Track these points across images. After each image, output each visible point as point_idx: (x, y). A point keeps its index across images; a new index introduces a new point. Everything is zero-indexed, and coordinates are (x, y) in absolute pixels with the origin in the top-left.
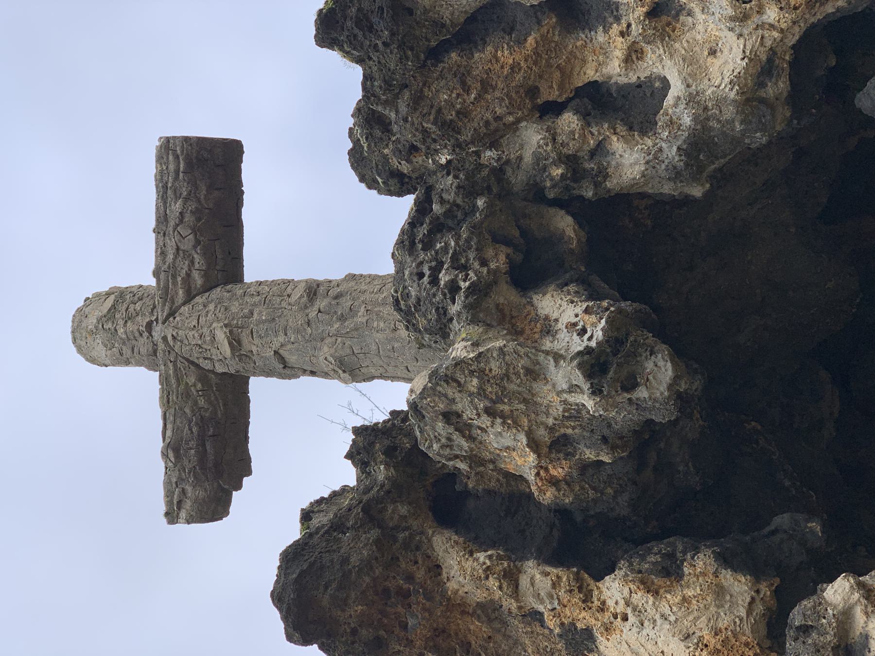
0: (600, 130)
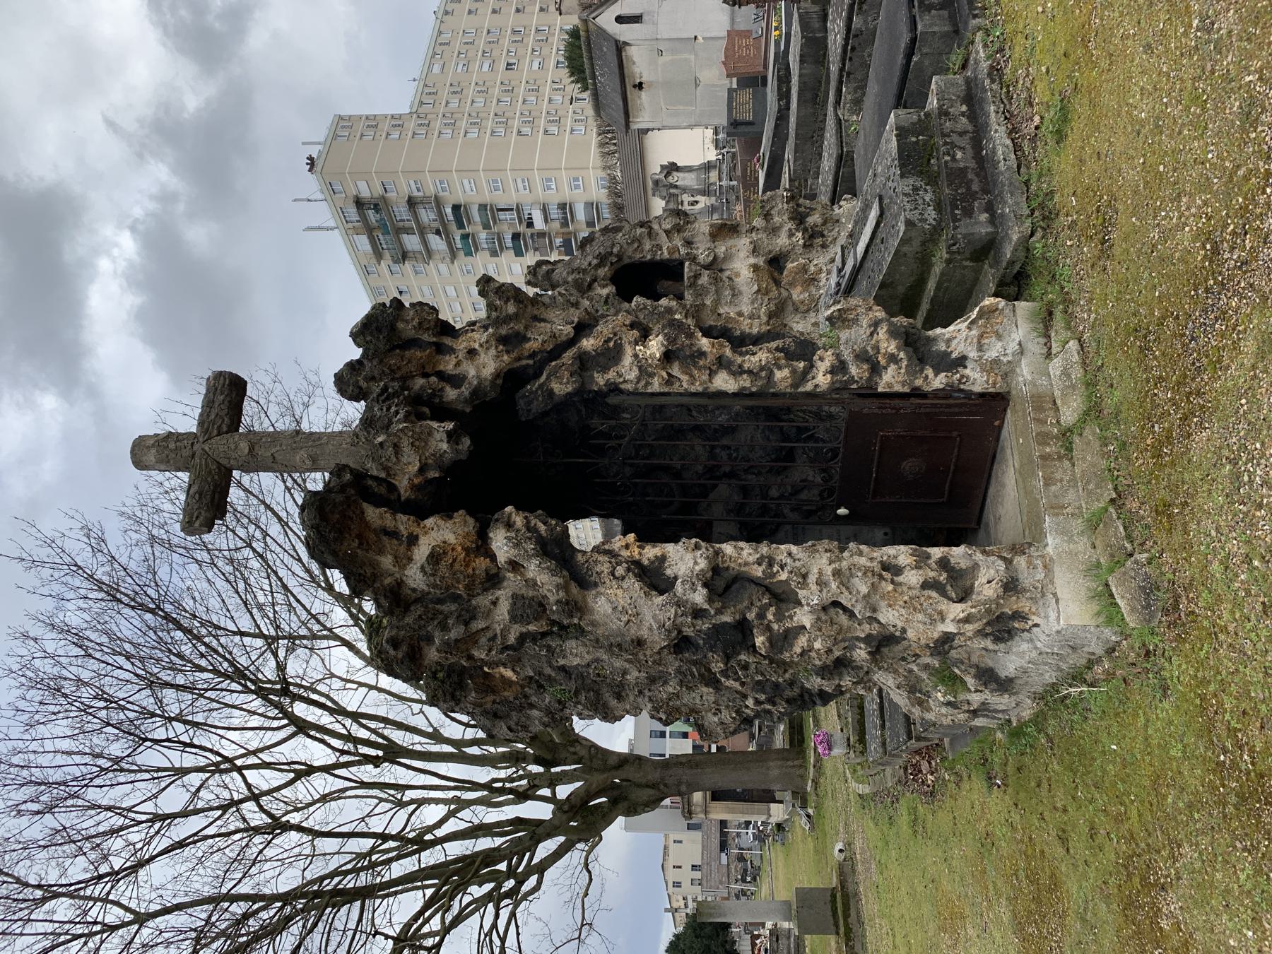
0: (442, 384)
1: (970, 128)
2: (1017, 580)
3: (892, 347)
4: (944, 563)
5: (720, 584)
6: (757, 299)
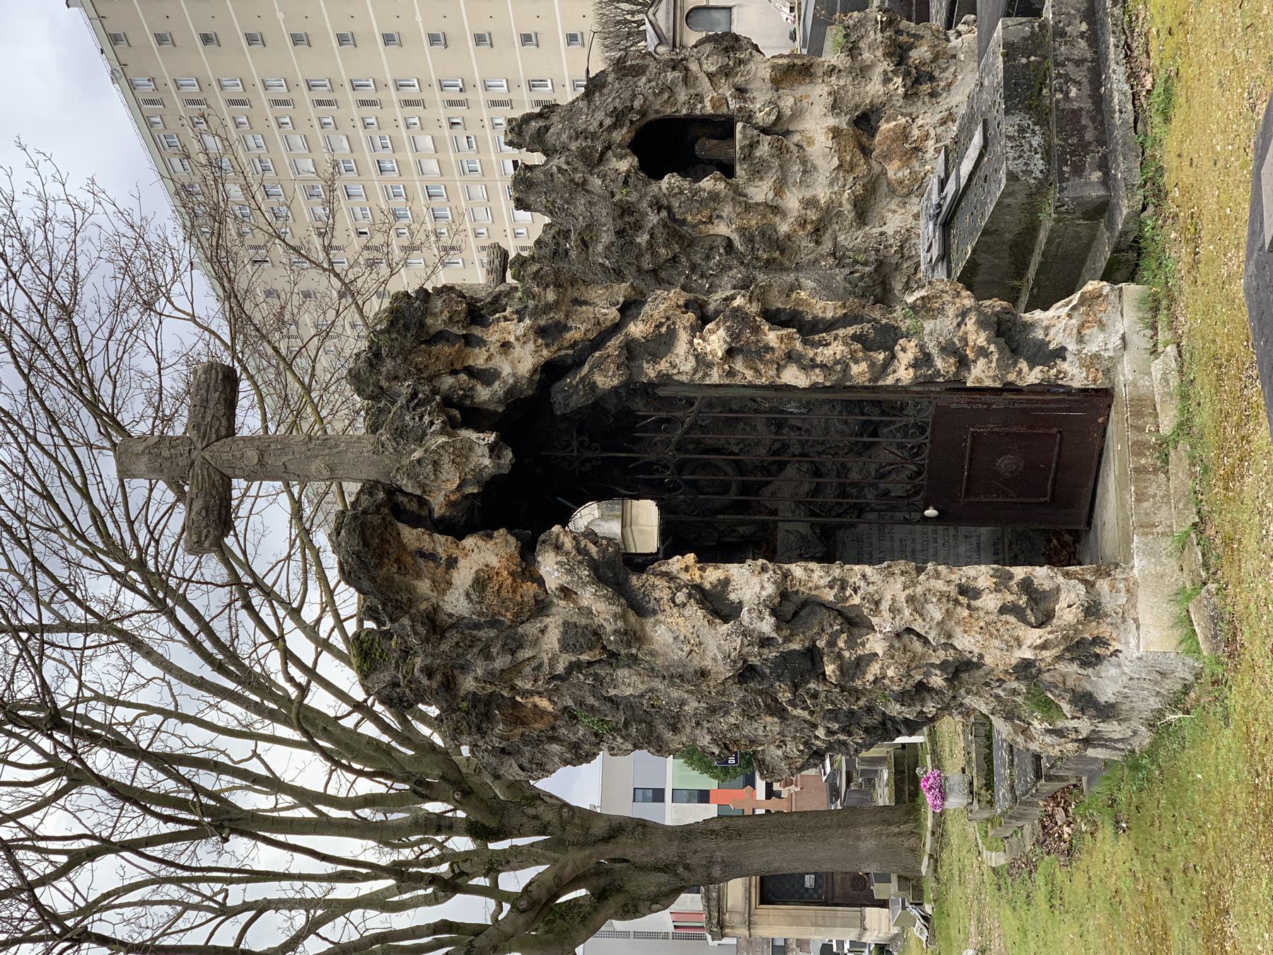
0: (474, 382)
1: (1089, 55)
2: (1100, 604)
3: (982, 340)
4: (1027, 586)
5: (789, 608)
6: (837, 179)
